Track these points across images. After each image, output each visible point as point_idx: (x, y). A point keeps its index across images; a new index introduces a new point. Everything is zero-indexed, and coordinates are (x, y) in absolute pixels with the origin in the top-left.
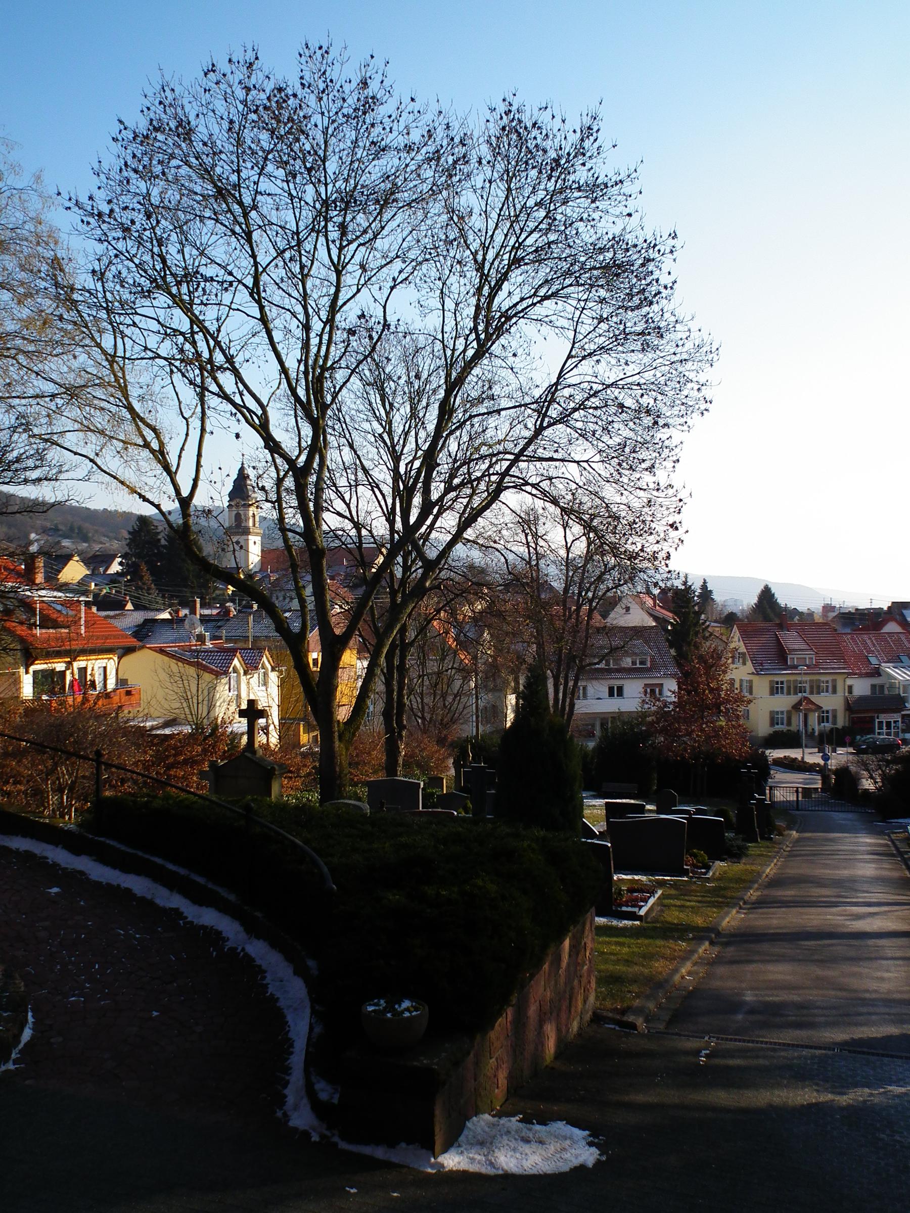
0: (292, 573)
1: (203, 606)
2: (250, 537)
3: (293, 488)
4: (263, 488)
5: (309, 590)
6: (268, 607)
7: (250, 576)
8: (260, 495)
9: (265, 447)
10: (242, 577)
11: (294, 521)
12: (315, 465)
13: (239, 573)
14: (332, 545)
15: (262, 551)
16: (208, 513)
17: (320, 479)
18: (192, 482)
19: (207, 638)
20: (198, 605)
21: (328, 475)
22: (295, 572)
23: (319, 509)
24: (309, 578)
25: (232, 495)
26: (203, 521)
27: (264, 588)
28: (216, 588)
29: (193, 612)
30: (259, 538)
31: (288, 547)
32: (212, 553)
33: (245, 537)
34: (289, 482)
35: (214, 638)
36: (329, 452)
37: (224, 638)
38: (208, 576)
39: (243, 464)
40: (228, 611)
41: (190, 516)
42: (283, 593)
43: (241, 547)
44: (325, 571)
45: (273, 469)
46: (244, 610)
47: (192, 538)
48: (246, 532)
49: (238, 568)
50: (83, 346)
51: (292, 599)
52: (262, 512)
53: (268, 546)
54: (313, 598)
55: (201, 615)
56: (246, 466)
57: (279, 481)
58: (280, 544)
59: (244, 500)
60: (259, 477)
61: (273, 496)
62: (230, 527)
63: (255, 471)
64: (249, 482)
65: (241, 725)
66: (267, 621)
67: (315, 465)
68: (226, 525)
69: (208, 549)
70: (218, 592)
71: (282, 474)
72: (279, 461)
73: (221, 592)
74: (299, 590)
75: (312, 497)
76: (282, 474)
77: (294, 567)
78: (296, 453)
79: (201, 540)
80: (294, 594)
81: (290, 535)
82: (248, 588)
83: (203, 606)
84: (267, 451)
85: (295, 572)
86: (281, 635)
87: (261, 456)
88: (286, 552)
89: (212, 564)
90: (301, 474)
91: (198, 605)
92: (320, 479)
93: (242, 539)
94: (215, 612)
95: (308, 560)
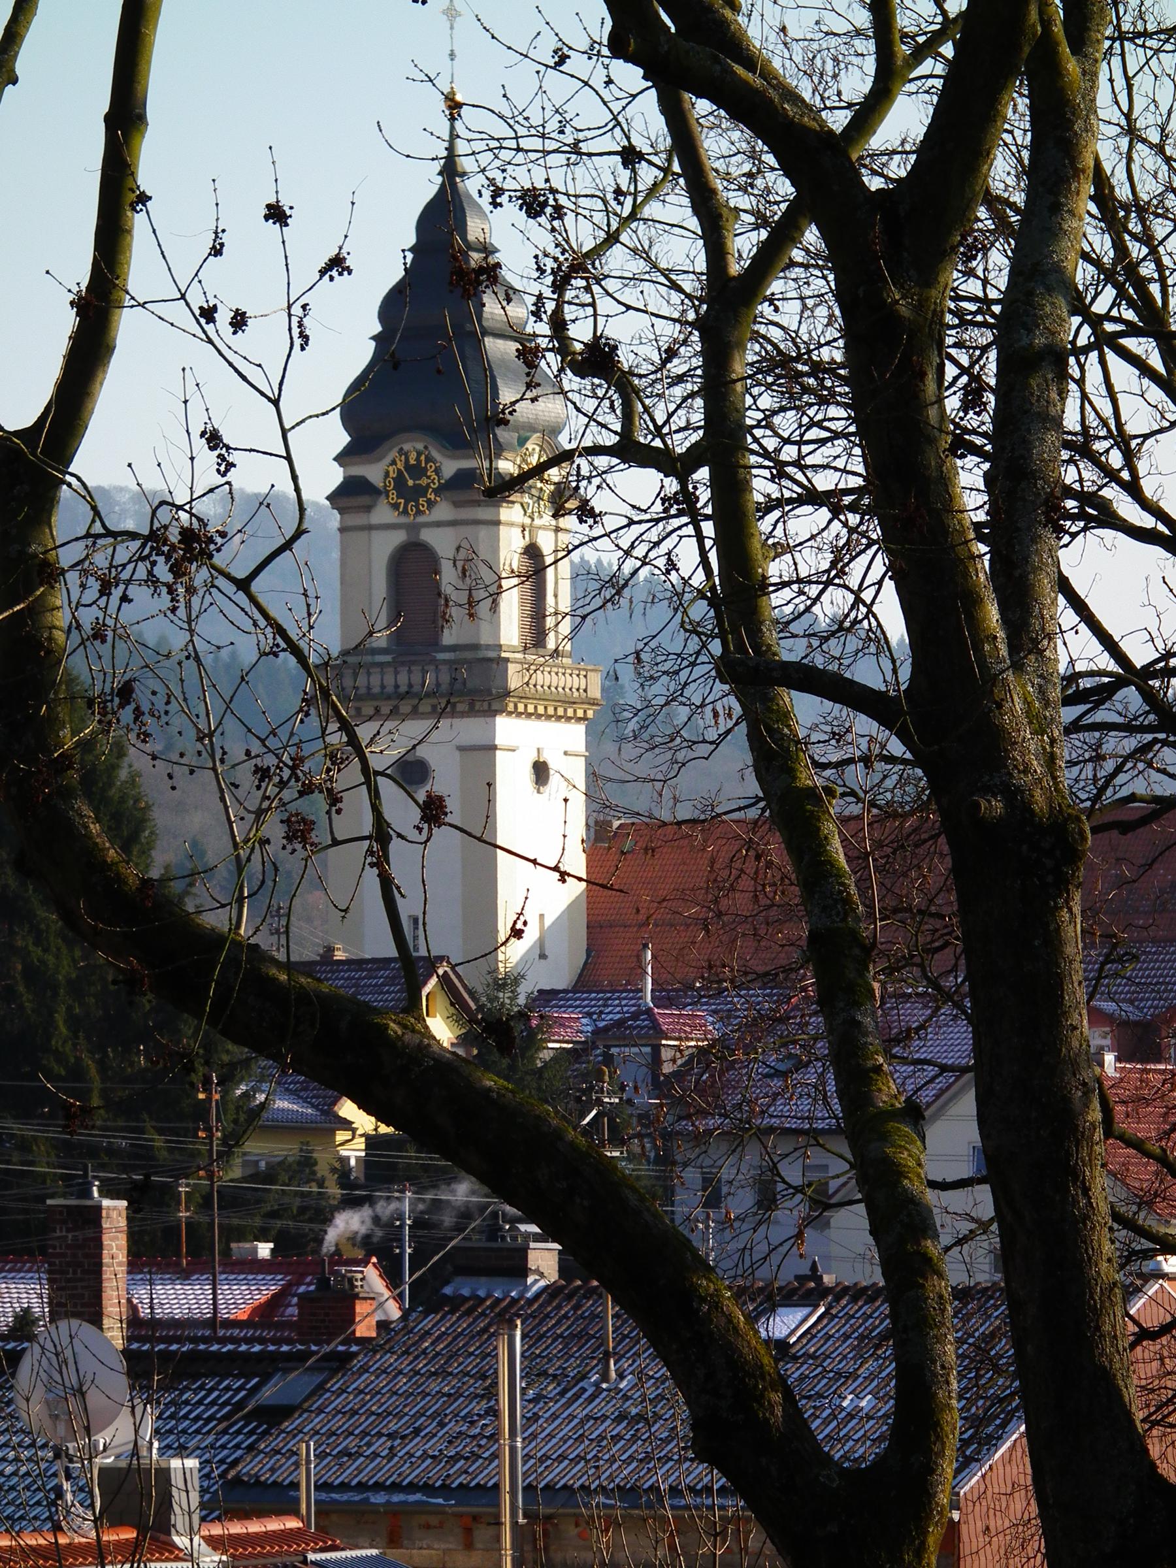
0: (826, 1001)
1: (153, 1254)
2: (506, 729)
3: (834, 354)
4: (599, 360)
5: (950, 1142)
6: (642, 1271)
7: (498, 1029)
8: (573, 413)
9: (619, 46)
10: (442, 1030)
11: (835, 602)
12: (1003, 173)
13: (412, 1006)
14: (1134, 783)
15: (600, 837)
16: (182, 547)
17: (1037, 274)
18: (68, 320)
19: (186, 1501)
20: (115, 1247)
21: (1101, 244)
22: (840, 993)
23: (1030, 508)
24: (954, 1040)
25: (369, 411)
26: (146, 613)
27: (613, 1121)
28: (251, 1119)
29: (79, 1296)
30: (574, 736)
31: (790, 804)
32: (217, 849)
33: (465, 729)
34: (801, 309)
35: (230, 1496)
36: (1108, 74)
37: (307, 1498)
38: (190, 1034)
39: (450, 169)
40: (339, 1302)
41: (50, 573)
42: (752, 1156)
43: (433, 811)
44: (1076, 991)
45: (675, 207)
46: (450, 1275)
47: (68, 740)
48: (477, 689)
49: (411, 968)
50: (828, 343)
51: (822, 1204)
52: (584, 543)
53: (640, 799)
54: (982, 1202)
55: (135, 1324)
56: (472, 185)
57: (726, 305)
58: (728, 778)
59: (457, 443)
60: (573, 269)
61: (681, 420)
62: (356, 654)
63: (540, 234)
64: (492, 307)
65: (503, 932)
66: (634, 1375)
67: (1003, 173)
68: (327, 637)
69: (189, 825)
70: (260, 1149)
71: (745, 243)
72: (724, 143)
73: (283, 1149)
74: (873, 1135)
75: (981, 421)
76: (745, 243)
77: (837, 957)
78: (857, 82)
79: (136, 759)
80: (836, 1166)
81: (806, 711)
82: (490, 1115)
83: (153, 1254)
84: (630, 75)
85: (840, 993)
86: (740, 1484)
87: (589, 113)
88: (775, 847)
89: (214, 941)
90: (895, 245)
91: (115, 1247)
92: (1037, 274)
93: (441, 743)
94: (240, 1298)
95: (948, 902)
